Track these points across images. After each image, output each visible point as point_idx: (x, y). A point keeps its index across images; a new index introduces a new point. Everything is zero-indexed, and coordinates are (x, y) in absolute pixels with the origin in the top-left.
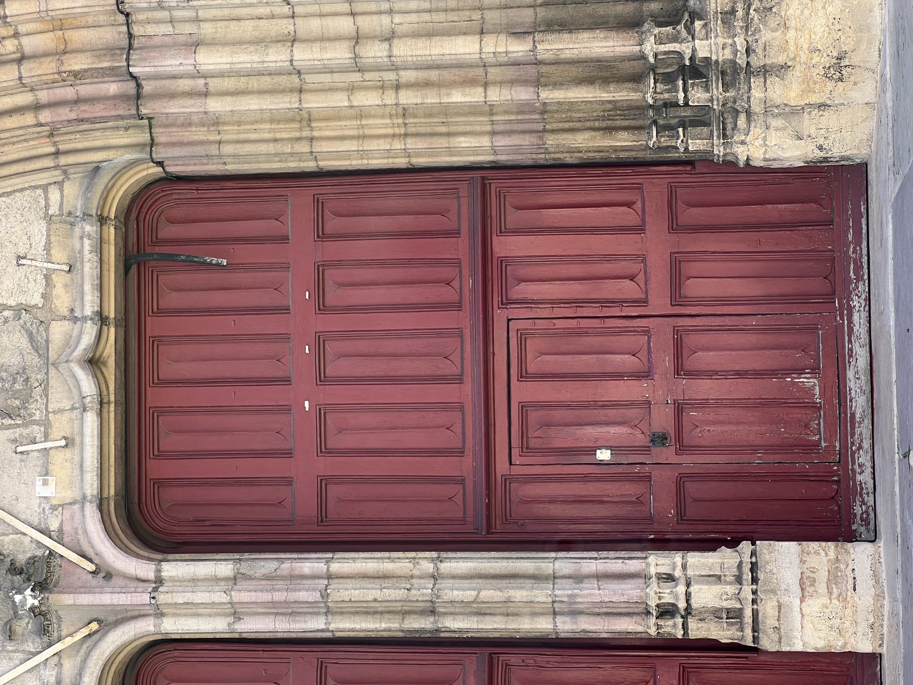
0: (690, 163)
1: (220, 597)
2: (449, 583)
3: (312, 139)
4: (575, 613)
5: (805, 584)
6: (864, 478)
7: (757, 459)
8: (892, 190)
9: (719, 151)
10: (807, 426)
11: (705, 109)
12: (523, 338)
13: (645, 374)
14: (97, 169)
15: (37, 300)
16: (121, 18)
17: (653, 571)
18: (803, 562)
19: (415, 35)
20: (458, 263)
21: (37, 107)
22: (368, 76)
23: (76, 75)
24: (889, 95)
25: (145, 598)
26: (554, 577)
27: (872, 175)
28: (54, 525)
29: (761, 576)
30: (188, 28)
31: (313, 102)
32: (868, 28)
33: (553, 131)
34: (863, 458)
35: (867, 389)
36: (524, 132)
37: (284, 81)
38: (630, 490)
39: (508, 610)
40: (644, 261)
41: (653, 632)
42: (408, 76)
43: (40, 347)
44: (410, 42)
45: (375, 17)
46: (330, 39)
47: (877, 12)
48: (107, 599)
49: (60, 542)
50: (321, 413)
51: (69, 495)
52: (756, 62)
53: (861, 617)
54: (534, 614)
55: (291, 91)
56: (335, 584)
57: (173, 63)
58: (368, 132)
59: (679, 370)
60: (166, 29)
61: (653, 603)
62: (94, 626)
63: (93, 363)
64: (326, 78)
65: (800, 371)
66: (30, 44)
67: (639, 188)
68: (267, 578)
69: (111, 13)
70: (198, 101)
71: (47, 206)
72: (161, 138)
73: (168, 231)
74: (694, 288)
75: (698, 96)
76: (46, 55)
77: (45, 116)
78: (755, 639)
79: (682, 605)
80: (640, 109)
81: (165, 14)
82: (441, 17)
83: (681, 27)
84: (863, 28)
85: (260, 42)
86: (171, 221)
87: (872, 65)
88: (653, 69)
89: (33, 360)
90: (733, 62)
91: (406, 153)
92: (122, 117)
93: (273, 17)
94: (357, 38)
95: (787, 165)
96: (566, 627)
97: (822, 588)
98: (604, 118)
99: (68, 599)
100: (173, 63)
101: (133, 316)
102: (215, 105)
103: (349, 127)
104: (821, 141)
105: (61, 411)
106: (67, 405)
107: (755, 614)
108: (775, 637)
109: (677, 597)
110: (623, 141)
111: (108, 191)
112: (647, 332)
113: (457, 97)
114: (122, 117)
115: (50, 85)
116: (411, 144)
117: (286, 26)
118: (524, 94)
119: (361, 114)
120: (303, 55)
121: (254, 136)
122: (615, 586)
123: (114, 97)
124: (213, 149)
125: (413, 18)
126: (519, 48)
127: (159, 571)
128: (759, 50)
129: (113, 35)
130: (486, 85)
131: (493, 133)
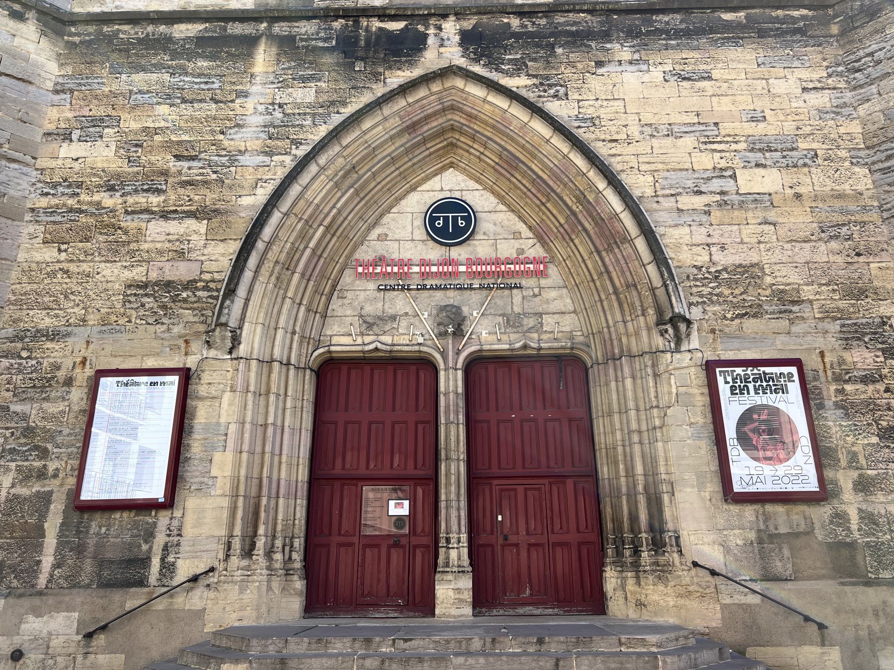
0: (603, 550)
1: (451, 389)
2: (456, 465)
3: (603, 416)
4: (447, 508)
5: (458, 590)
6: (495, 612)
7: (500, 574)
8: (598, 624)
9: (608, 560)
10: (512, 592)
11: (623, 555)
12: (539, 489)
13: (528, 533)
14: (589, 346)
15: (545, 329)
16: (640, 353)
17: (461, 535)
18: (466, 589)
19: (642, 452)
20: (405, 469)
21: (608, 327)
22: (627, 436)
23: (620, 339)
24: (632, 623)
25: (451, 365)
26: (459, 501)
27: (602, 617)
28: (473, 337)
29: (460, 574)
30: (639, 375)
31: (616, 417)
32: (656, 616)
33: (611, 500)
34: (501, 612)
35: (526, 614)
37: (623, 407)
38: (488, 528)
39: (448, 485)
40: (567, 533)
41: (441, 535)
42: (628, 449)
43: (529, 330)
44: (640, 450)
46: (639, 422)
47: (662, 619)
48: (450, 353)
49: (468, 338)
50: (511, 421)
51: (483, 340)
52: (641, 574)
53: (447, 610)
54: (446, 494)
55: (620, 410)
56: (455, 426)
57: (627, 370)
59: (530, 545)
60: (638, 368)
61: (451, 535)
62: (442, 350)
63: (525, 347)
64: (625, 421)
65: (531, 590)
66: (630, 324)
67: (593, 531)
68: (457, 404)
69: (642, 350)
70: (614, 379)
72: (600, 367)
73: (569, 370)
74: (559, 550)
75: (627, 553)
76: (626, 330)
77: (605, 330)
78: (439, 572)
79: (450, 546)
80: (621, 531)
81: (643, 367)
82: (649, 460)
83: (651, 547)
84: (656, 614)
85: (636, 399)
86: (572, 370)
87: (642, 616)
88: (636, 536)
89: (525, 328)
90: (640, 566)
91: (600, 449)
92: (607, 354)
94: (640, 432)
95: (604, 585)
96: (443, 505)
97: (457, 596)
98: (617, 519)
99: (450, 342)
100: (627, 370)
101: (541, 359)
102: (613, 384)
103: (608, 429)
104: (613, 598)
105: (509, 337)
106: (511, 339)
107: (448, 572)
108: (440, 579)
109: (453, 544)
110: (610, 525)
111: (582, 350)
112: (542, 534)
113: (621, 466)
114: (607, 354)
115: (616, 331)
116: (604, 451)
117: (642, 407)
118: (624, 490)
119: (613, 433)
120: (633, 413)
121: (603, 397)
122: (456, 522)
123: (613, 352)
124: (598, 384)
125: (648, 451)
126: (640, 488)
127: (459, 369)
128: (645, 575)
129: (634, 350)
130: (626, 476)
131: (609, 479)
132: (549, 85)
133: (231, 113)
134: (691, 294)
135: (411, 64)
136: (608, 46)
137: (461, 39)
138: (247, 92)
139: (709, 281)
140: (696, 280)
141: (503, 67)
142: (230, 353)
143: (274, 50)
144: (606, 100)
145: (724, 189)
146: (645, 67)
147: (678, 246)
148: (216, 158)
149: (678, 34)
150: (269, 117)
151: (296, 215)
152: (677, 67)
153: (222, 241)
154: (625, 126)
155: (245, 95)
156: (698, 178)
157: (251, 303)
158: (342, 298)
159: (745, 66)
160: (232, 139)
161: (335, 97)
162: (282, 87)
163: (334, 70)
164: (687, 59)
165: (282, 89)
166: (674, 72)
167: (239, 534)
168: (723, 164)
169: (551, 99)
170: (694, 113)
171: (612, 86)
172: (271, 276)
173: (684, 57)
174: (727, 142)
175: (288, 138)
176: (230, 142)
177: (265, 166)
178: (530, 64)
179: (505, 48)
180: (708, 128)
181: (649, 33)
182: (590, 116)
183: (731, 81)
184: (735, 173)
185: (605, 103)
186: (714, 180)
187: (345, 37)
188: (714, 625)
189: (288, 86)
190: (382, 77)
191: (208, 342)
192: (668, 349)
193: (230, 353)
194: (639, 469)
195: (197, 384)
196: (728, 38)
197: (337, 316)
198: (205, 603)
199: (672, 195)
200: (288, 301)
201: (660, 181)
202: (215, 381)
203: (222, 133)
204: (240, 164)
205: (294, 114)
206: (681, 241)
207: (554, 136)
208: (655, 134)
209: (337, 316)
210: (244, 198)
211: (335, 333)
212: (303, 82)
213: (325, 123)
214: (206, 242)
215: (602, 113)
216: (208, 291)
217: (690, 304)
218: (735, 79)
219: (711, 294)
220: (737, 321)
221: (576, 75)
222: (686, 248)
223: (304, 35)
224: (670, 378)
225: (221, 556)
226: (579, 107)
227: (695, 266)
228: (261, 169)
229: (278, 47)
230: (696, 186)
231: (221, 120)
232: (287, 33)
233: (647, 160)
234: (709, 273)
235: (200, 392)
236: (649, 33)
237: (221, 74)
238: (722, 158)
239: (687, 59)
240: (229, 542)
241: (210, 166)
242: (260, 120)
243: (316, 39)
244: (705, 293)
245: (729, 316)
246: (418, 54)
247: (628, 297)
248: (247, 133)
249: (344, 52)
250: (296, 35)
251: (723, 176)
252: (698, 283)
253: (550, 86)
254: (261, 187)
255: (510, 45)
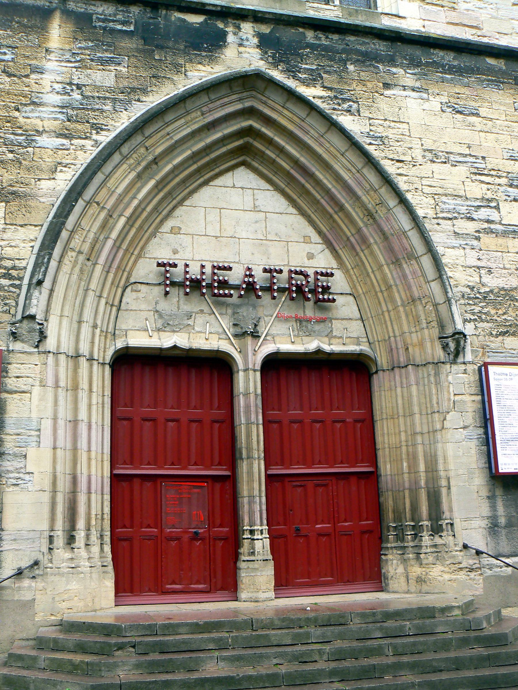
15: (334, 334)
31: (401, 420)
33: (393, 494)
36: (392, 485)
45: (428, 440)
49: (264, 340)
55: (404, 413)
57: (412, 378)
58: (390, 436)
69: (425, 360)
71: (361, 338)
72: (385, 373)
81: (426, 375)
93: (427, 408)
100: (412, 378)
102: (399, 390)
116: (387, 450)
132: (342, 99)
133: (27, 89)
134: (466, 311)
135: (212, 60)
136: (394, 70)
137: (260, 42)
138: (42, 68)
139: (479, 300)
140: (469, 298)
141: (300, 75)
142: (37, 347)
143: (70, 27)
144: (393, 121)
145: (491, 218)
146: (425, 96)
147: (455, 266)
148: (12, 137)
149: (451, 70)
150: (66, 97)
151: (98, 204)
152: (452, 100)
153: (21, 226)
154: (410, 148)
155: (40, 71)
156: (470, 206)
157: (55, 294)
158: (136, 291)
159: (505, 109)
160: (28, 118)
161: (135, 84)
162: (80, 68)
163: (133, 55)
164: (459, 94)
165: (80, 70)
166: (449, 104)
167: (61, 528)
168: (489, 195)
169: (345, 113)
170: (466, 146)
171: (397, 109)
172: (74, 267)
173: (458, 92)
174: (492, 176)
175: (88, 122)
176: (26, 120)
177: (64, 149)
178: (325, 76)
179: (301, 56)
180: (477, 161)
181: (427, 64)
182: (380, 135)
183: (494, 121)
184: (498, 205)
185: (392, 124)
186: (482, 209)
187: (144, 22)
188: (478, 593)
189: (86, 67)
190: (183, 69)
191: (13, 334)
192: (448, 360)
193: (37, 347)
194: (422, 467)
195: (5, 377)
196: (492, 81)
197: (131, 310)
198: (33, 594)
199: (450, 219)
200: (91, 293)
201: (440, 204)
202: (24, 375)
203: (18, 110)
204: (37, 145)
205: (93, 97)
206: (457, 262)
207: (350, 151)
208: (435, 160)
209: (131, 310)
210: (43, 182)
211: (130, 327)
212: (102, 65)
213: (126, 110)
214: (4, 226)
215: (390, 133)
216: (10, 279)
217: (465, 321)
218: (497, 119)
219: (480, 312)
220: (500, 338)
221: (367, 94)
222: (461, 269)
223: (101, 15)
224: (449, 387)
225: (45, 549)
226: (370, 125)
227: (469, 286)
228: (60, 152)
229: (75, 24)
230: (469, 213)
231: (16, 95)
232: (83, 10)
233: (428, 183)
234: (480, 293)
235: (8, 385)
236: (427, 64)
237: (13, 46)
238: (488, 190)
239: (459, 94)
240: (51, 537)
241: (6, 145)
242: (56, 99)
243: (114, 21)
244: (476, 311)
245: (494, 333)
246: (218, 51)
247: (413, 310)
248: (45, 112)
249: (144, 39)
250: (93, 14)
251: (489, 206)
252: (471, 302)
253: (344, 100)
254: (61, 171)
255: (306, 55)
